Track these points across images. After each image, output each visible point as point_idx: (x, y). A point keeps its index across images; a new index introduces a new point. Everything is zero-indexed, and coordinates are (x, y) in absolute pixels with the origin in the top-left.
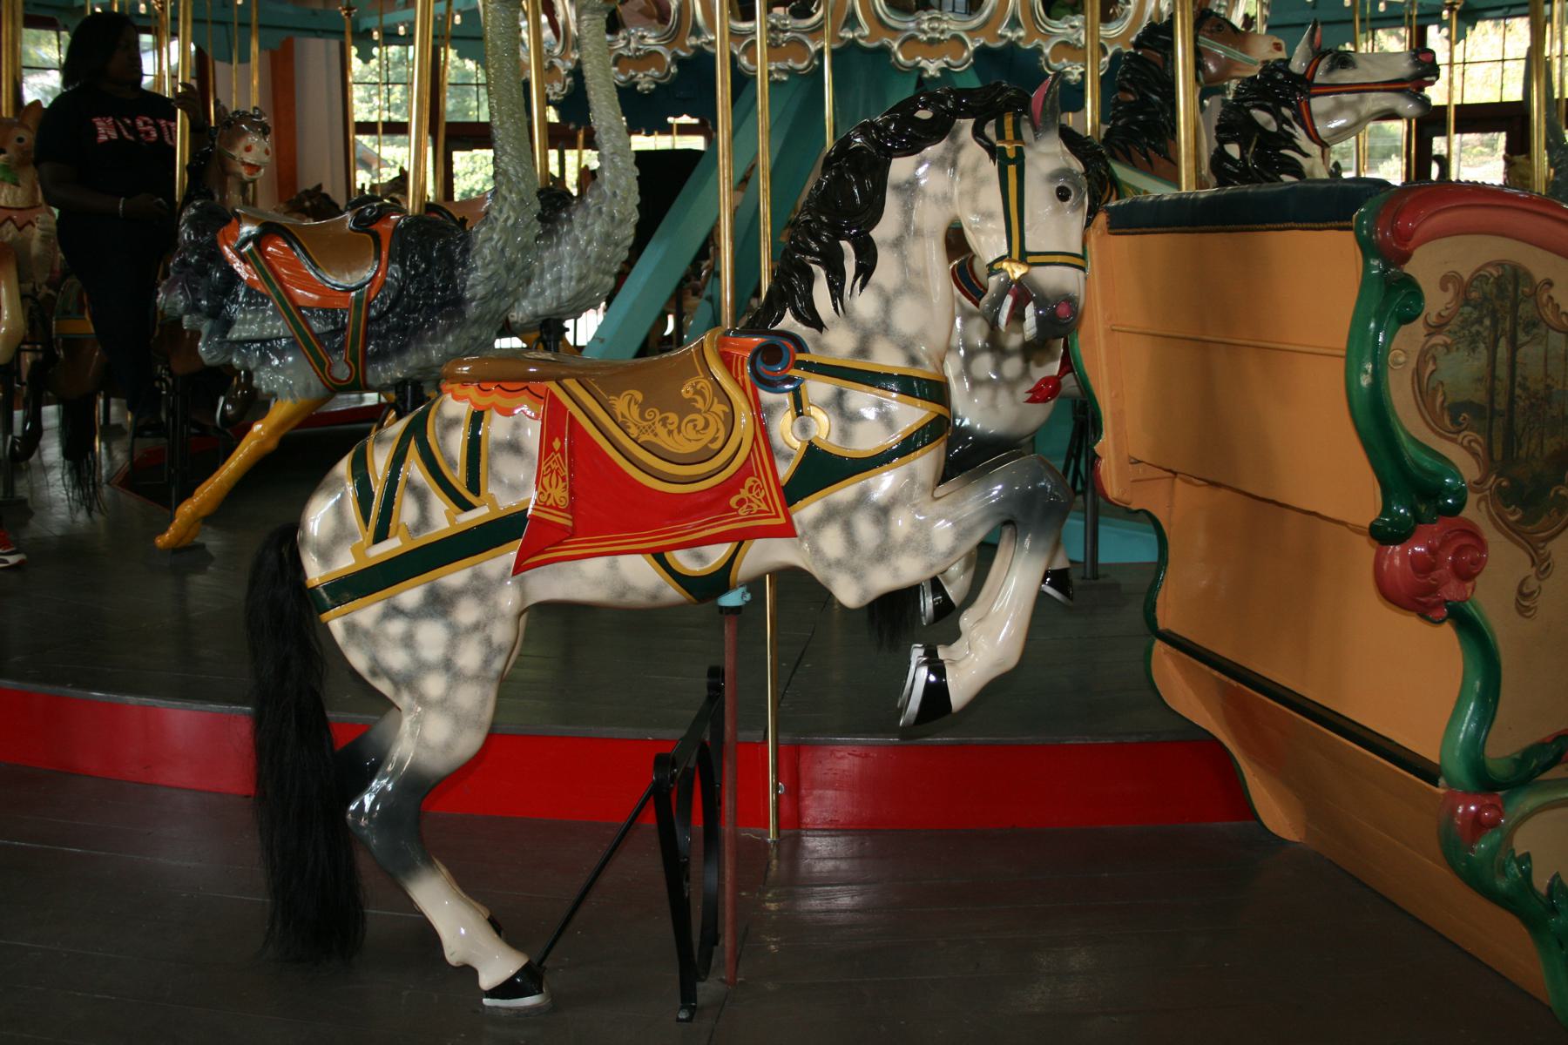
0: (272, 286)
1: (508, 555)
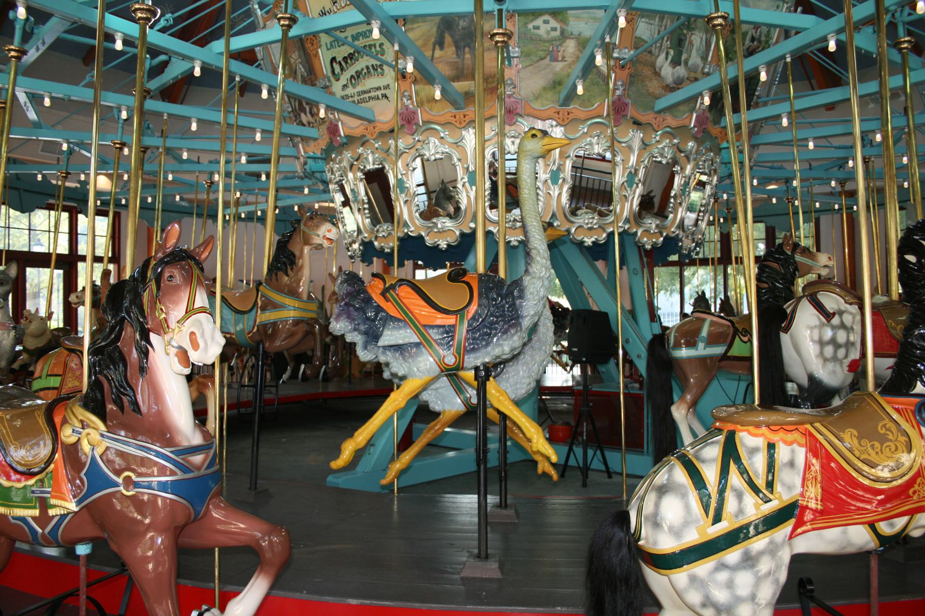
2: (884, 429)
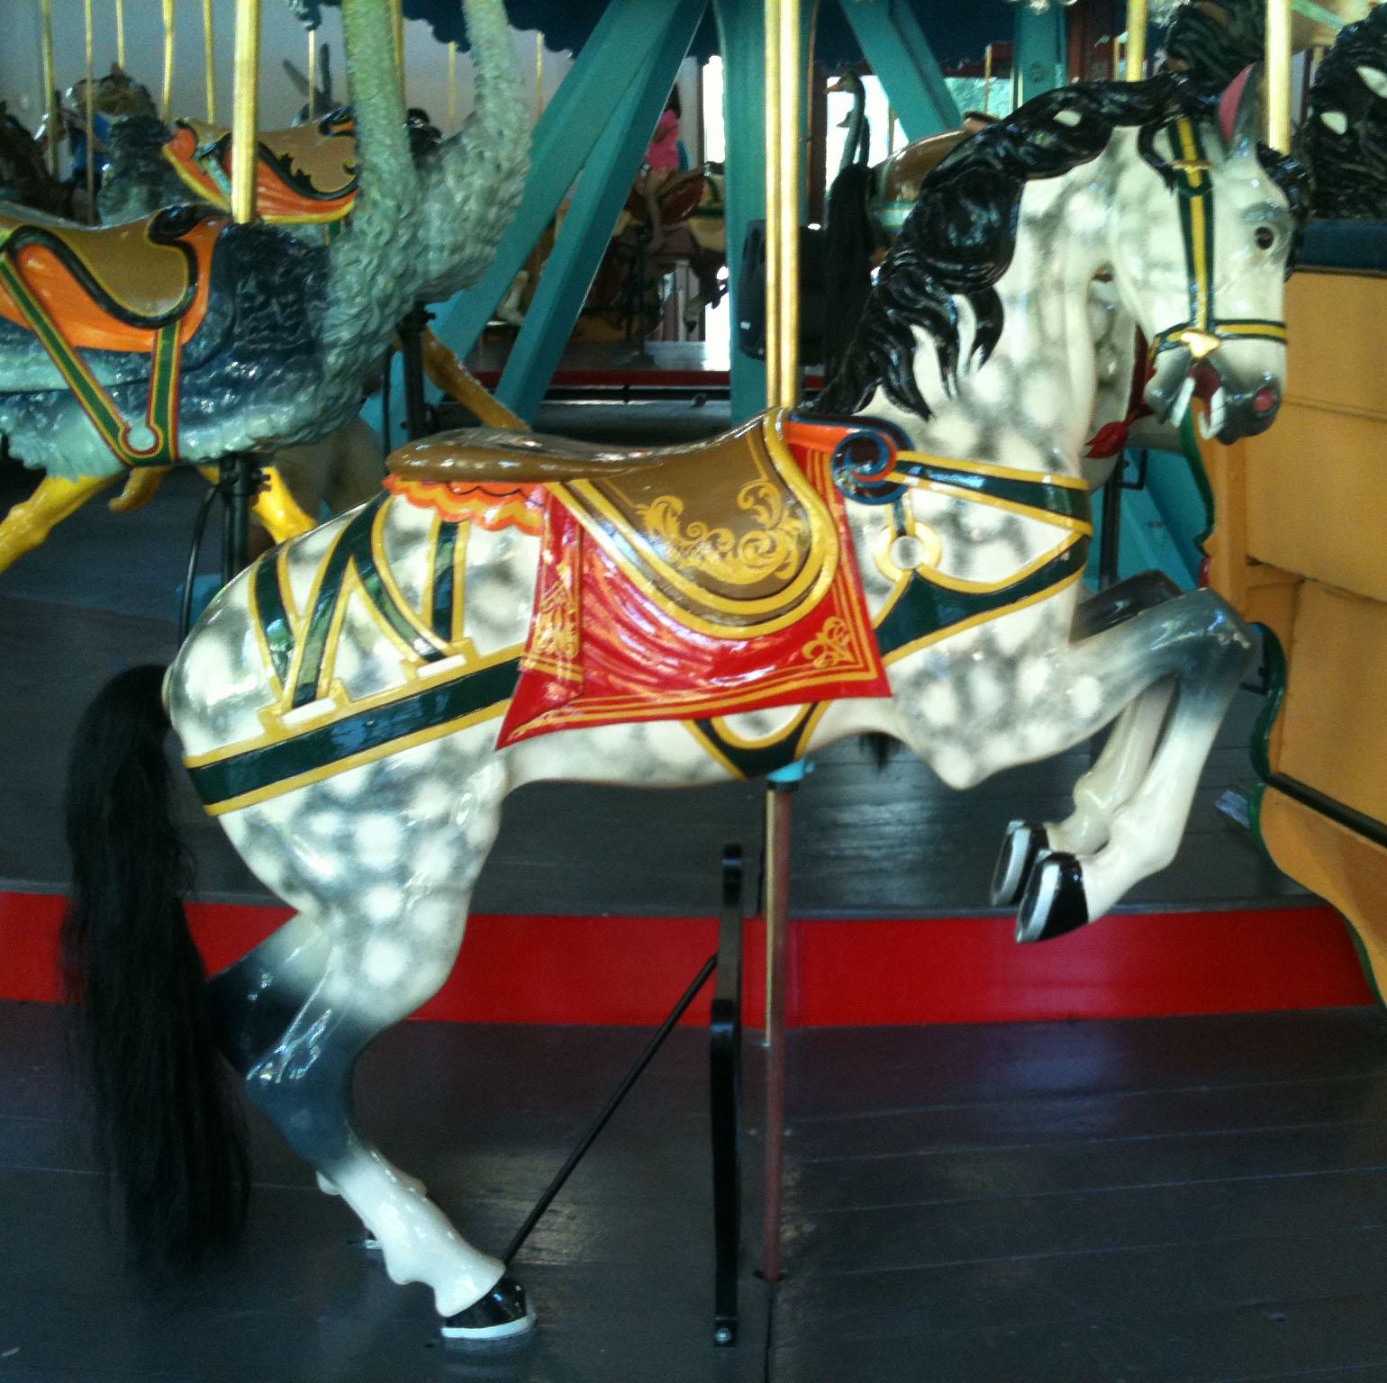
0: (38, 319)
1: (487, 725)
2: (751, 500)
